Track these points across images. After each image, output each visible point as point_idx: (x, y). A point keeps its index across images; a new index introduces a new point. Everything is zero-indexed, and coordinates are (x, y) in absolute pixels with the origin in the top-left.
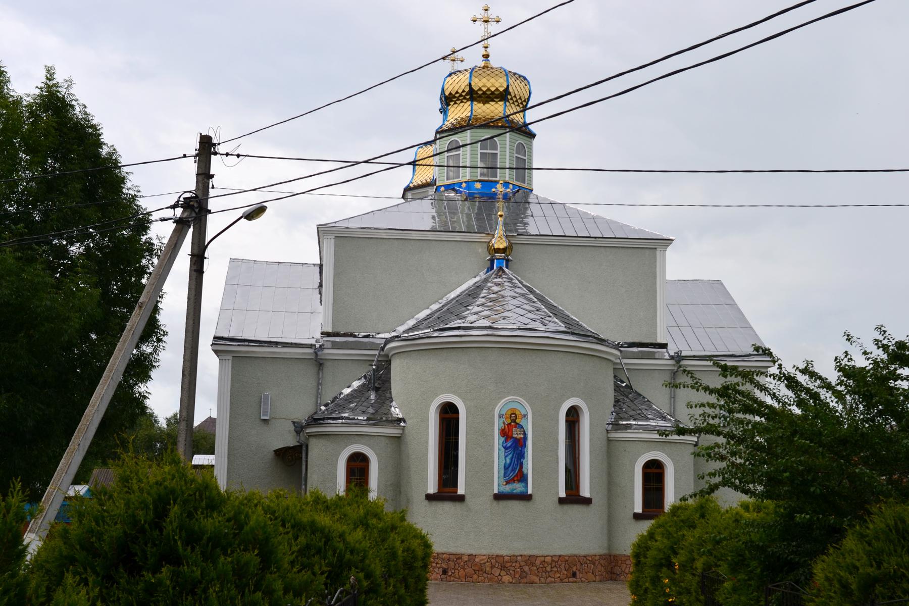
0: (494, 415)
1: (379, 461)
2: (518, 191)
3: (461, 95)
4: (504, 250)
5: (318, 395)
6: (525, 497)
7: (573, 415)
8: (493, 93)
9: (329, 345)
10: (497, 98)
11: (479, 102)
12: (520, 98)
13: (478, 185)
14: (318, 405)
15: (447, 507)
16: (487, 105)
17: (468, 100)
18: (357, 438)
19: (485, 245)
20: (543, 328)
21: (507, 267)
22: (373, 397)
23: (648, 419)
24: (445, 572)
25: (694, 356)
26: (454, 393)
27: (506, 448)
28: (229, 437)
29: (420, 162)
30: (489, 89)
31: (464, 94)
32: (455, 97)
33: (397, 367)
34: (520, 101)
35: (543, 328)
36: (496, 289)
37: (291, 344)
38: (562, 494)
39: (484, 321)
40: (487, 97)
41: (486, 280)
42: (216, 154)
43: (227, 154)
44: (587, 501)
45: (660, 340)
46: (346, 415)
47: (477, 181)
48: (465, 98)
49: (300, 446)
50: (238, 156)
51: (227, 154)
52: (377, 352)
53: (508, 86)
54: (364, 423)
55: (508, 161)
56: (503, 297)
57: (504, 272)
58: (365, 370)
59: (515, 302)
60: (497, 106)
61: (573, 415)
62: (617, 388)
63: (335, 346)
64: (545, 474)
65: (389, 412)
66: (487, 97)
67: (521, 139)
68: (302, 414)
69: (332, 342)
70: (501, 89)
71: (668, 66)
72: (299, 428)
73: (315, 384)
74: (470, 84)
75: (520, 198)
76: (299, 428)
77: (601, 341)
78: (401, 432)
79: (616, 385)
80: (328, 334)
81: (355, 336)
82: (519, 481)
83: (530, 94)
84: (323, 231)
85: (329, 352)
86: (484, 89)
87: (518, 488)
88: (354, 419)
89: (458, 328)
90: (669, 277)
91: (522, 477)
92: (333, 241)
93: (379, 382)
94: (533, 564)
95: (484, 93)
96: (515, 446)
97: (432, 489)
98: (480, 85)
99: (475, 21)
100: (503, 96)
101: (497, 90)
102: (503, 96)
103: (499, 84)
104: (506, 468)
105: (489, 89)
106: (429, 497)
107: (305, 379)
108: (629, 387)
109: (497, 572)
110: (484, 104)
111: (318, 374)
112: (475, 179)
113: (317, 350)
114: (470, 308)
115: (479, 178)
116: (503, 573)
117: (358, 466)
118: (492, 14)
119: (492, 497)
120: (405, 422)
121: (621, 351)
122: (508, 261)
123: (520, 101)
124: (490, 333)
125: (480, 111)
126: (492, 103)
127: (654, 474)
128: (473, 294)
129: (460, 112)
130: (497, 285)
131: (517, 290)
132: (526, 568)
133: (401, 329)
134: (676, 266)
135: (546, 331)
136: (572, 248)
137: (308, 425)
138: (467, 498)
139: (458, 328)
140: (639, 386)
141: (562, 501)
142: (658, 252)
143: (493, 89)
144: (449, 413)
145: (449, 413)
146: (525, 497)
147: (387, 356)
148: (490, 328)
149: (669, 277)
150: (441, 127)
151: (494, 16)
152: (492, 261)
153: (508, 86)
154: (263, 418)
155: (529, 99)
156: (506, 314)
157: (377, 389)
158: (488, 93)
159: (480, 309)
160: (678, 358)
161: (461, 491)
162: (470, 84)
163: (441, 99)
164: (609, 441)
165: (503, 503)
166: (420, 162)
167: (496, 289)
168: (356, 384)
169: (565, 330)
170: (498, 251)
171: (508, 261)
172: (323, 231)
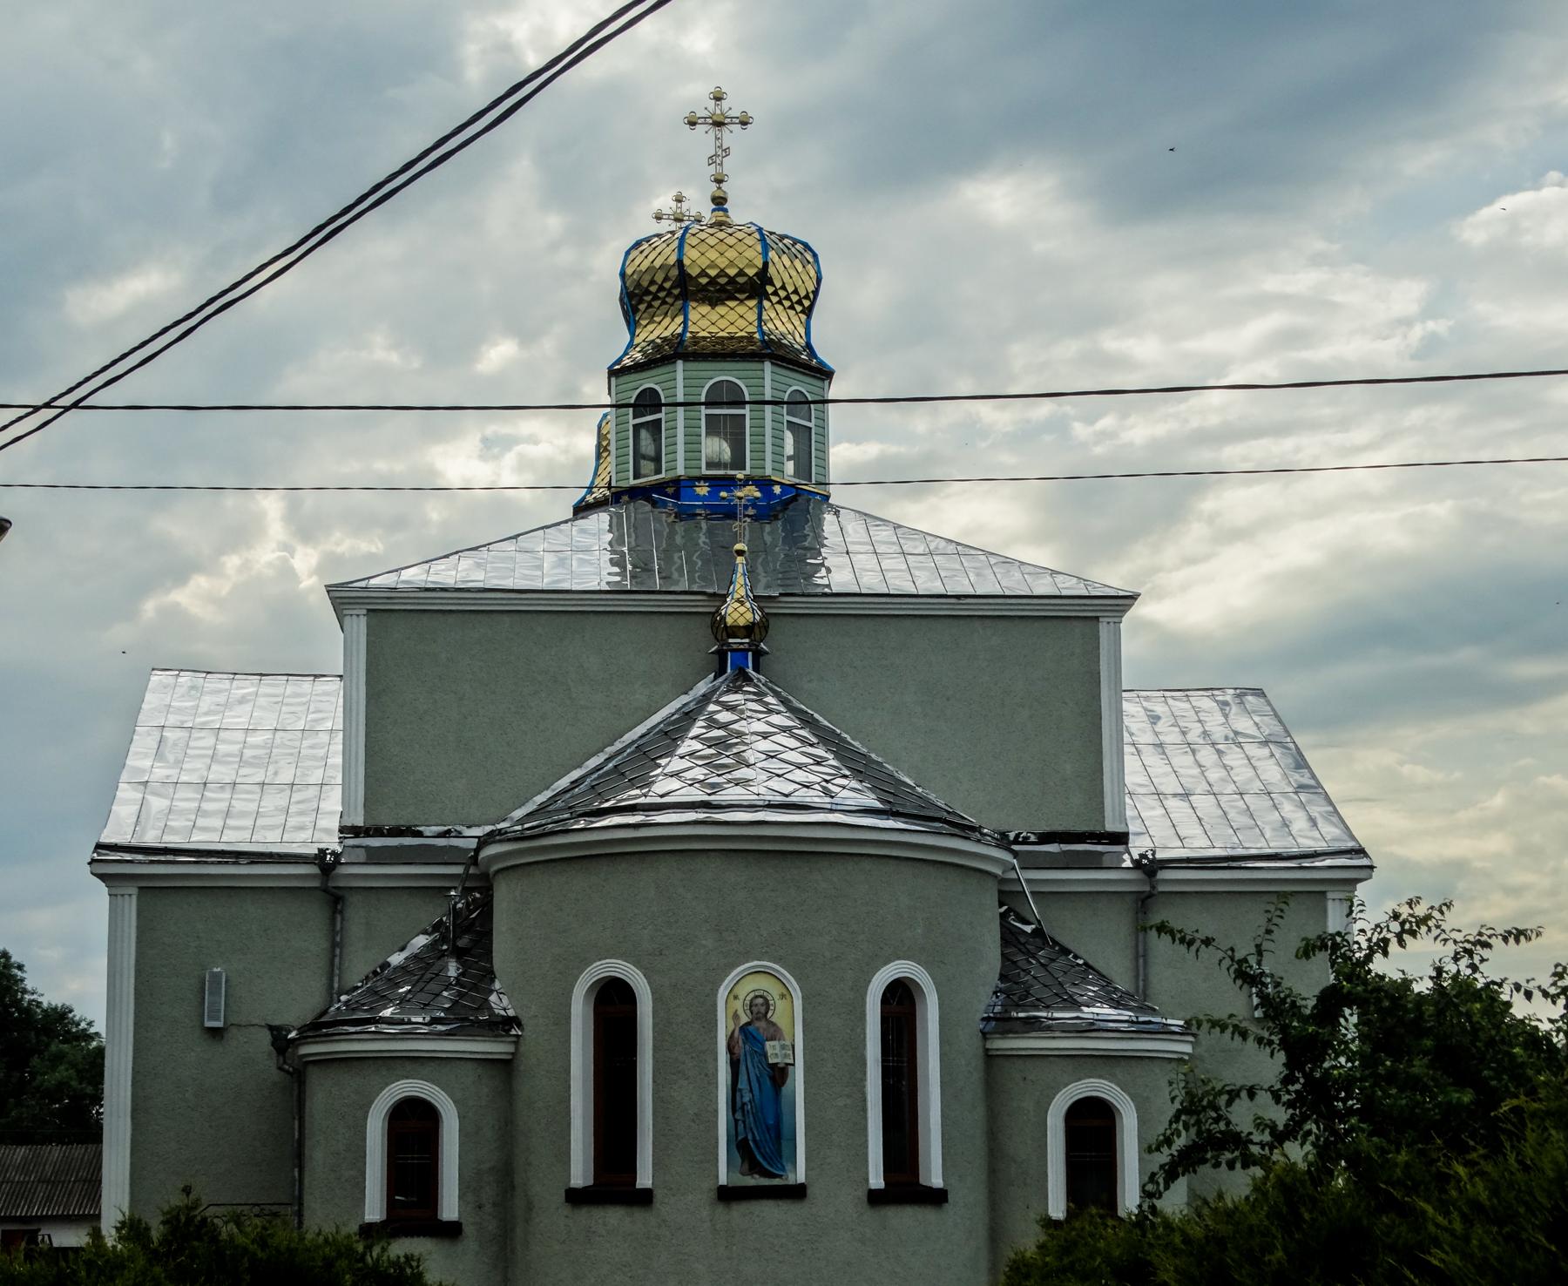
0: (715, 1005)
1: (461, 1118)
2: (794, 499)
3: (661, 288)
4: (749, 630)
5: (333, 967)
7: (901, 998)
8: (732, 280)
9: (361, 856)
10: (741, 291)
11: (702, 301)
12: (796, 292)
13: (703, 490)
14: (331, 995)
15: (613, 1217)
16: (721, 310)
17: (677, 298)
18: (409, 1066)
19: (708, 620)
21: (756, 669)
22: (453, 970)
23: (1076, 1005)
25: (1189, 860)
26: (625, 957)
28: (135, 1072)
29: (24, 411)
30: (722, 273)
31: (667, 285)
32: (647, 292)
33: (505, 897)
34: (795, 298)
36: (725, 717)
37: (279, 855)
38: (877, 1181)
39: (738, 789)
40: (720, 290)
41: (706, 699)
44: (937, 1198)
45: (1111, 826)
46: (387, 1013)
47: (699, 479)
48: (669, 294)
52: (459, 870)
53: (766, 265)
54: (425, 1030)
55: (680, 423)
56: (740, 734)
57: (749, 680)
58: (435, 912)
59: (765, 745)
60: (741, 309)
61: (901, 998)
62: (1009, 937)
63: (375, 857)
64: (834, 1146)
65: (485, 1005)
66: (720, 290)
67: (798, 384)
68: (295, 1011)
69: (367, 848)
70: (751, 272)
71: (438, 154)
73: (325, 945)
74: (680, 263)
75: (794, 509)
77: (966, 830)
78: (511, 1049)
80: (356, 831)
81: (420, 834)
83: (819, 280)
85: (353, 871)
86: (713, 273)
88: (402, 1022)
89: (632, 809)
92: (363, 620)
93: (468, 935)
95: (713, 281)
97: (580, 1173)
98: (704, 263)
99: (692, 124)
100: (757, 287)
101: (741, 273)
102: (757, 287)
103: (749, 258)
105: (722, 273)
106: (576, 1197)
107: (306, 935)
110: (713, 305)
111: (333, 920)
112: (695, 473)
113: (324, 863)
114: (663, 762)
115: (705, 472)
118: (732, 106)
119: (714, 1195)
120: (520, 1025)
121: (1016, 854)
122: (758, 654)
123: (795, 298)
124: (701, 816)
125: (704, 323)
126: (732, 304)
127: (1092, 1128)
129: (664, 328)
131: (776, 719)
135: (831, 811)
136: (908, 623)
137: (303, 1038)
138: (658, 1195)
139: (632, 809)
140: (1068, 928)
141: (876, 1198)
142: (1104, 629)
143: (732, 272)
144: (614, 1001)
145: (614, 1001)
150: (619, 361)
151: (735, 113)
152: (721, 655)
153: (766, 265)
154: (208, 1024)
155: (816, 292)
156: (743, 773)
157: (459, 954)
158: (723, 281)
159: (685, 764)
160: (1149, 867)
161: (936, 1180)
162: (680, 263)
163: (621, 300)
164: (990, 1058)
165: (740, 1210)
166: (24, 411)
167: (725, 717)
168: (421, 941)
169: (878, 805)
170: (734, 631)
171: (758, 654)
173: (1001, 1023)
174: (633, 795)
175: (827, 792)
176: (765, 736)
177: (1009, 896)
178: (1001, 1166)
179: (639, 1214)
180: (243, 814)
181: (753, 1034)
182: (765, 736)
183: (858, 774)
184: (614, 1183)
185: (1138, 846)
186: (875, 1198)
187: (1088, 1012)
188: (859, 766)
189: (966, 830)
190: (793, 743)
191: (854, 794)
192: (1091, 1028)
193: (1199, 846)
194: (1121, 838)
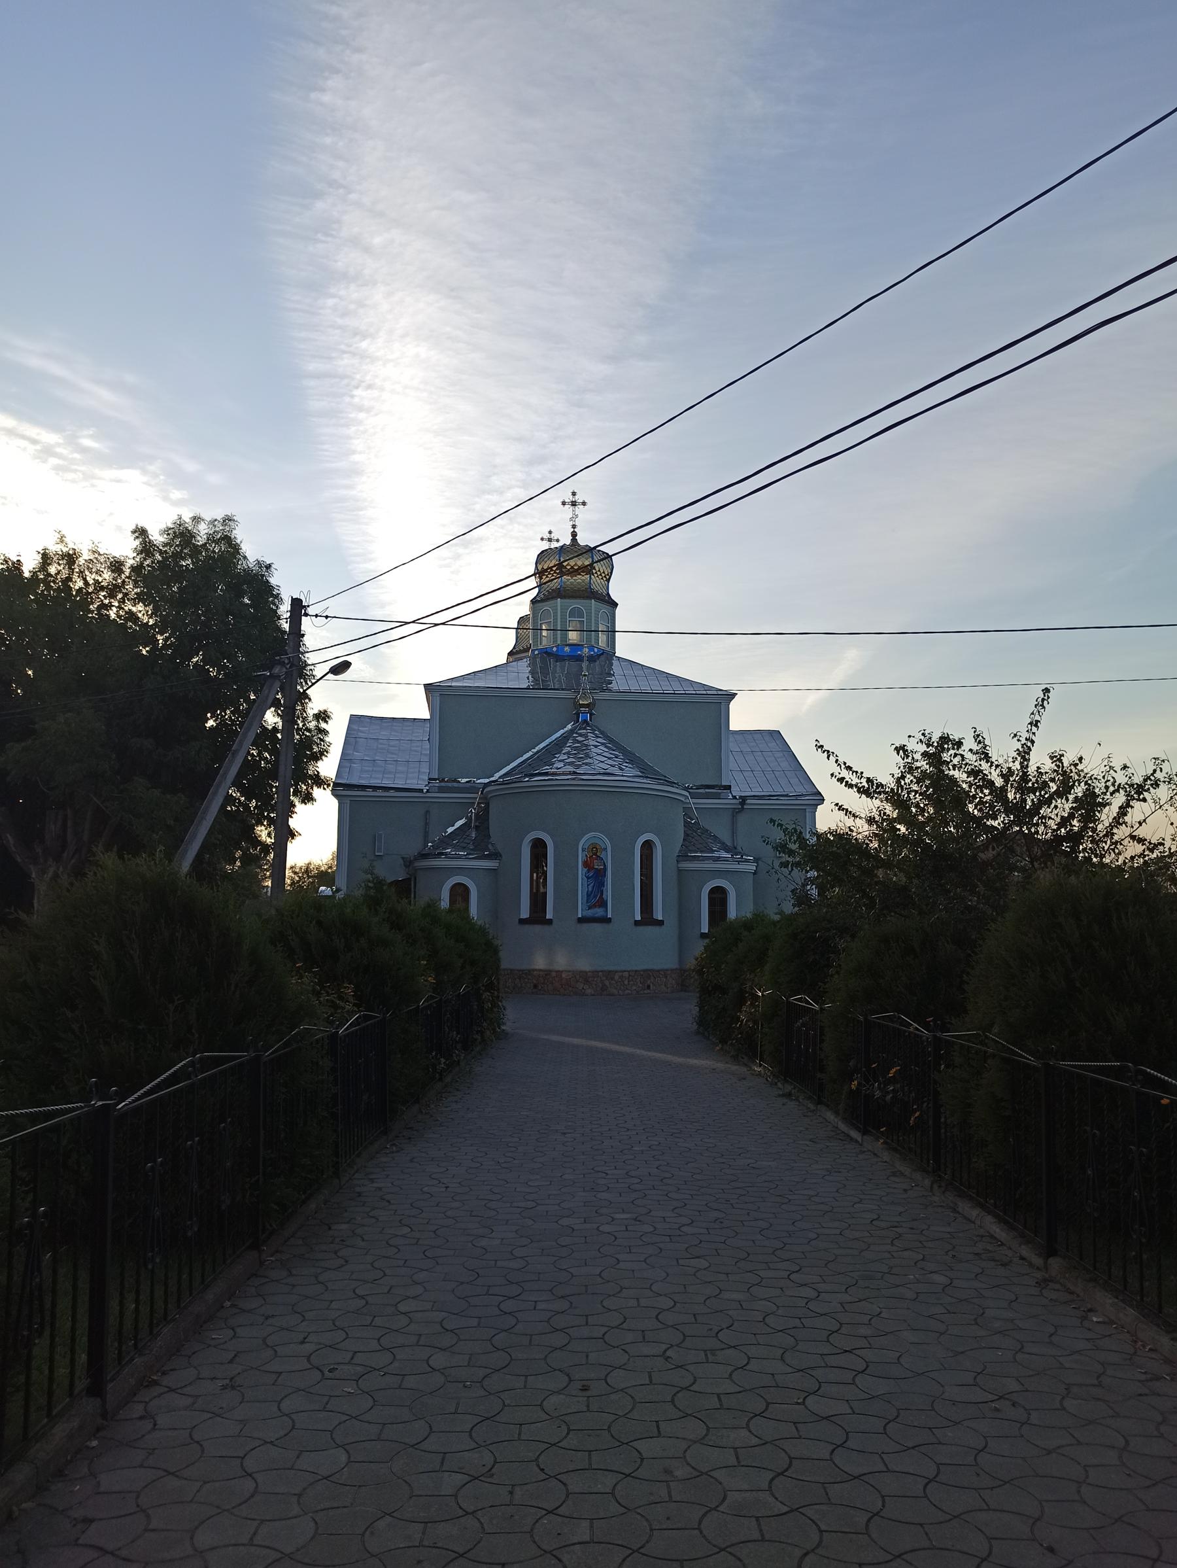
6: (606, 920)
7: (648, 846)
15: (537, 928)
20: (619, 772)
23: (713, 851)
24: (535, 986)
27: (588, 878)
35: (619, 772)
36: (580, 739)
38: (638, 918)
41: (572, 731)
42: (306, 615)
43: (316, 616)
44: (661, 923)
49: (409, 879)
50: (327, 617)
51: (316, 616)
61: (648, 846)
64: (624, 898)
68: (412, 847)
72: (408, 863)
76: (408, 863)
79: (685, 822)
82: (600, 906)
84: (429, 688)
87: (599, 912)
89: (546, 774)
90: (733, 726)
91: (603, 904)
93: (482, 822)
94: (612, 979)
96: (597, 876)
97: (525, 913)
104: (588, 895)
106: (522, 922)
108: (697, 823)
109: (580, 986)
116: (586, 987)
117: (460, 892)
127: (718, 898)
128: (559, 745)
130: (581, 735)
132: (607, 983)
133: (497, 775)
134: (741, 718)
137: (416, 859)
139: (546, 774)
145: (539, 848)
146: (606, 920)
147: (486, 798)
148: (575, 773)
149: (733, 726)
156: (589, 761)
161: (660, 918)
164: (679, 871)
167: (580, 739)
172: (429, 688)
173: (683, 857)
174: (546, 769)
175: (621, 769)
176: (596, 746)
177: (687, 812)
178: (685, 911)
179: (546, 927)
180: (390, 773)
181: (595, 852)
182: (596, 746)
183: (631, 762)
184: (538, 915)
185: (736, 792)
186: (637, 923)
187: (716, 854)
188: (632, 759)
189: (671, 784)
190: (603, 759)
191: (630, 771)
192: (718, 859)
193: (757, 791)
194: (729, 787)
